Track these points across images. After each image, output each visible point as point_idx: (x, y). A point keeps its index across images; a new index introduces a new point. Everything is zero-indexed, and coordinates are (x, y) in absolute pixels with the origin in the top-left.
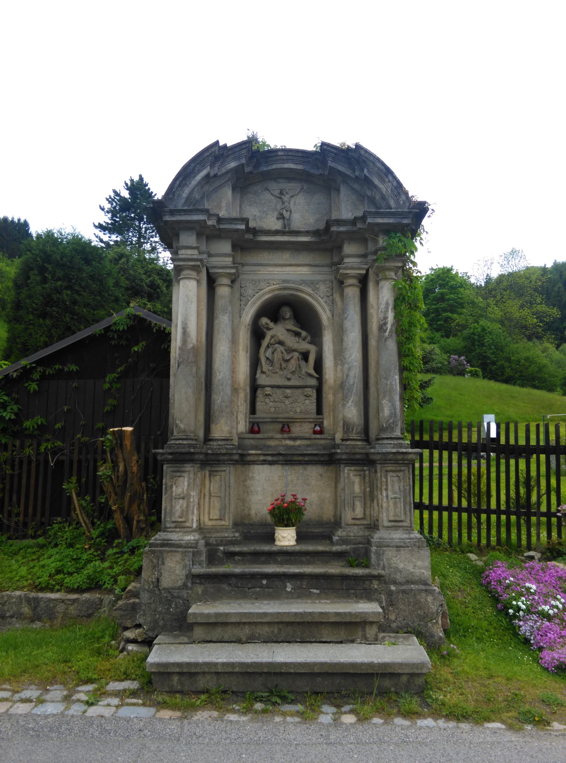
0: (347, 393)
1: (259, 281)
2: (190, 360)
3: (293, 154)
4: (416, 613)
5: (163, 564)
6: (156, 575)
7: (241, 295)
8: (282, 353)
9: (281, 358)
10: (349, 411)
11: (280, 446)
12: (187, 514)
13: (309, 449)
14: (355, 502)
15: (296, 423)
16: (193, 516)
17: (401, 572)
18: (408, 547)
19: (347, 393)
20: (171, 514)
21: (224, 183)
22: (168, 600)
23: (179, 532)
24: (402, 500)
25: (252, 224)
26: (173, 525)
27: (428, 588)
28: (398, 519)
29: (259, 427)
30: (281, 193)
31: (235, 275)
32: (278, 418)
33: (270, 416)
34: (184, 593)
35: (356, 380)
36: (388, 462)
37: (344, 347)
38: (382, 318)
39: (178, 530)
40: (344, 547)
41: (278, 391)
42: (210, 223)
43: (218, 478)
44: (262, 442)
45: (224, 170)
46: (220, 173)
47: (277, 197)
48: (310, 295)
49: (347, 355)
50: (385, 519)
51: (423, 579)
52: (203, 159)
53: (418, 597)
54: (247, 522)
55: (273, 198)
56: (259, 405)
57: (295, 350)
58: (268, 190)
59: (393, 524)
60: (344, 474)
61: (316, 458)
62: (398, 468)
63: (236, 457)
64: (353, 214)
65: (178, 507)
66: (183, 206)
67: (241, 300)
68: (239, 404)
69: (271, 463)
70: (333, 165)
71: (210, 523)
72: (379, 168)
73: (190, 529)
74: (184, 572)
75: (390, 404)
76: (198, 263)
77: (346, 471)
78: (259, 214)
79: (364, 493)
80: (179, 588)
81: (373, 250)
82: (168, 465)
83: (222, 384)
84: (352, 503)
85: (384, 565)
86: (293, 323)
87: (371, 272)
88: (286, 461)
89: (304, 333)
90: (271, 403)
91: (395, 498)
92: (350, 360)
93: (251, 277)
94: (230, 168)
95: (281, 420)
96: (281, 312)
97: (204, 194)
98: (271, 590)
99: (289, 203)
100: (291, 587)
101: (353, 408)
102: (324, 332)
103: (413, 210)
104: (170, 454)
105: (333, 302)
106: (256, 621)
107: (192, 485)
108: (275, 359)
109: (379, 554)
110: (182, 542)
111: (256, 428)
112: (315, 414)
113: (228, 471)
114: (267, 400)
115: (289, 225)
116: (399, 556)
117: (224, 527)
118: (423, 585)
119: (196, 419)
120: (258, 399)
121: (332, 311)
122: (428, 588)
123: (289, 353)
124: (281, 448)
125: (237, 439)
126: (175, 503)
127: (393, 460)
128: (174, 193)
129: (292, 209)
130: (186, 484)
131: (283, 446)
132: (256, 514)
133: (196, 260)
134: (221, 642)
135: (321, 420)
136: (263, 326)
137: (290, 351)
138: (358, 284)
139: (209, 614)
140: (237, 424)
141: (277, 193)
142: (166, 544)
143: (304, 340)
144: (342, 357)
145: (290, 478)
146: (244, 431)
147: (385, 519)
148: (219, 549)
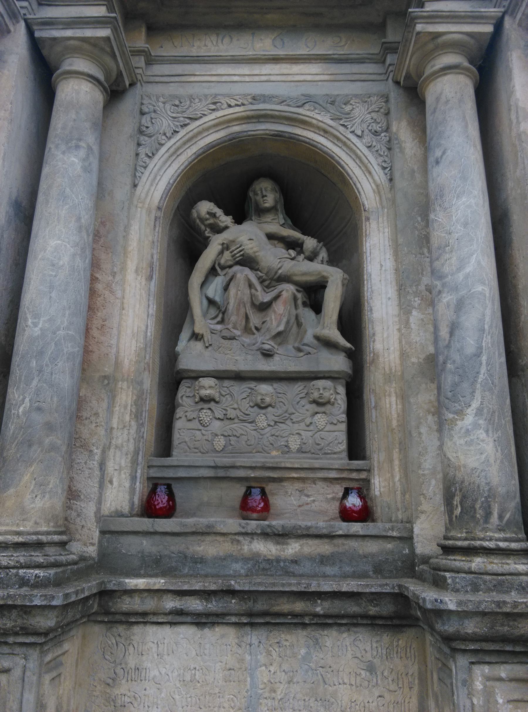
0: (456, 385)
1: (191, 98)
8: (251, 286)
9: (247, 298)
10: (469, 443)
11: (236, 560)
13: (329, 570)
15: (285, 484)
19: (456, 385)
29: (171, 496)
32: (233, 467)
33: (209, 460)
35: (487, 341)
60: (470, 695)
61: (353, 608)
67: (139, 145)
68: (115, 423)
77: (479, 685)
83: (41, 353)
86: (282, 221)
88: (250, 615)
89: (310, 243)
90: (217, 424)
92: (461, 276)
93: (172, 89)
95: (241, 473)
96: (251, 194)
102: (365, 226)
108: (232, 301)
111: (162, 500)
112: (345, 455)
113: (17, 672)
114: (205, 415)
120: (179, 412)
123: (268, 287)
124: (237, 566)
125: (97, 534)
131: (246, 560)
135: (363, 475)
136: (202, 220)
146: (126, 509)
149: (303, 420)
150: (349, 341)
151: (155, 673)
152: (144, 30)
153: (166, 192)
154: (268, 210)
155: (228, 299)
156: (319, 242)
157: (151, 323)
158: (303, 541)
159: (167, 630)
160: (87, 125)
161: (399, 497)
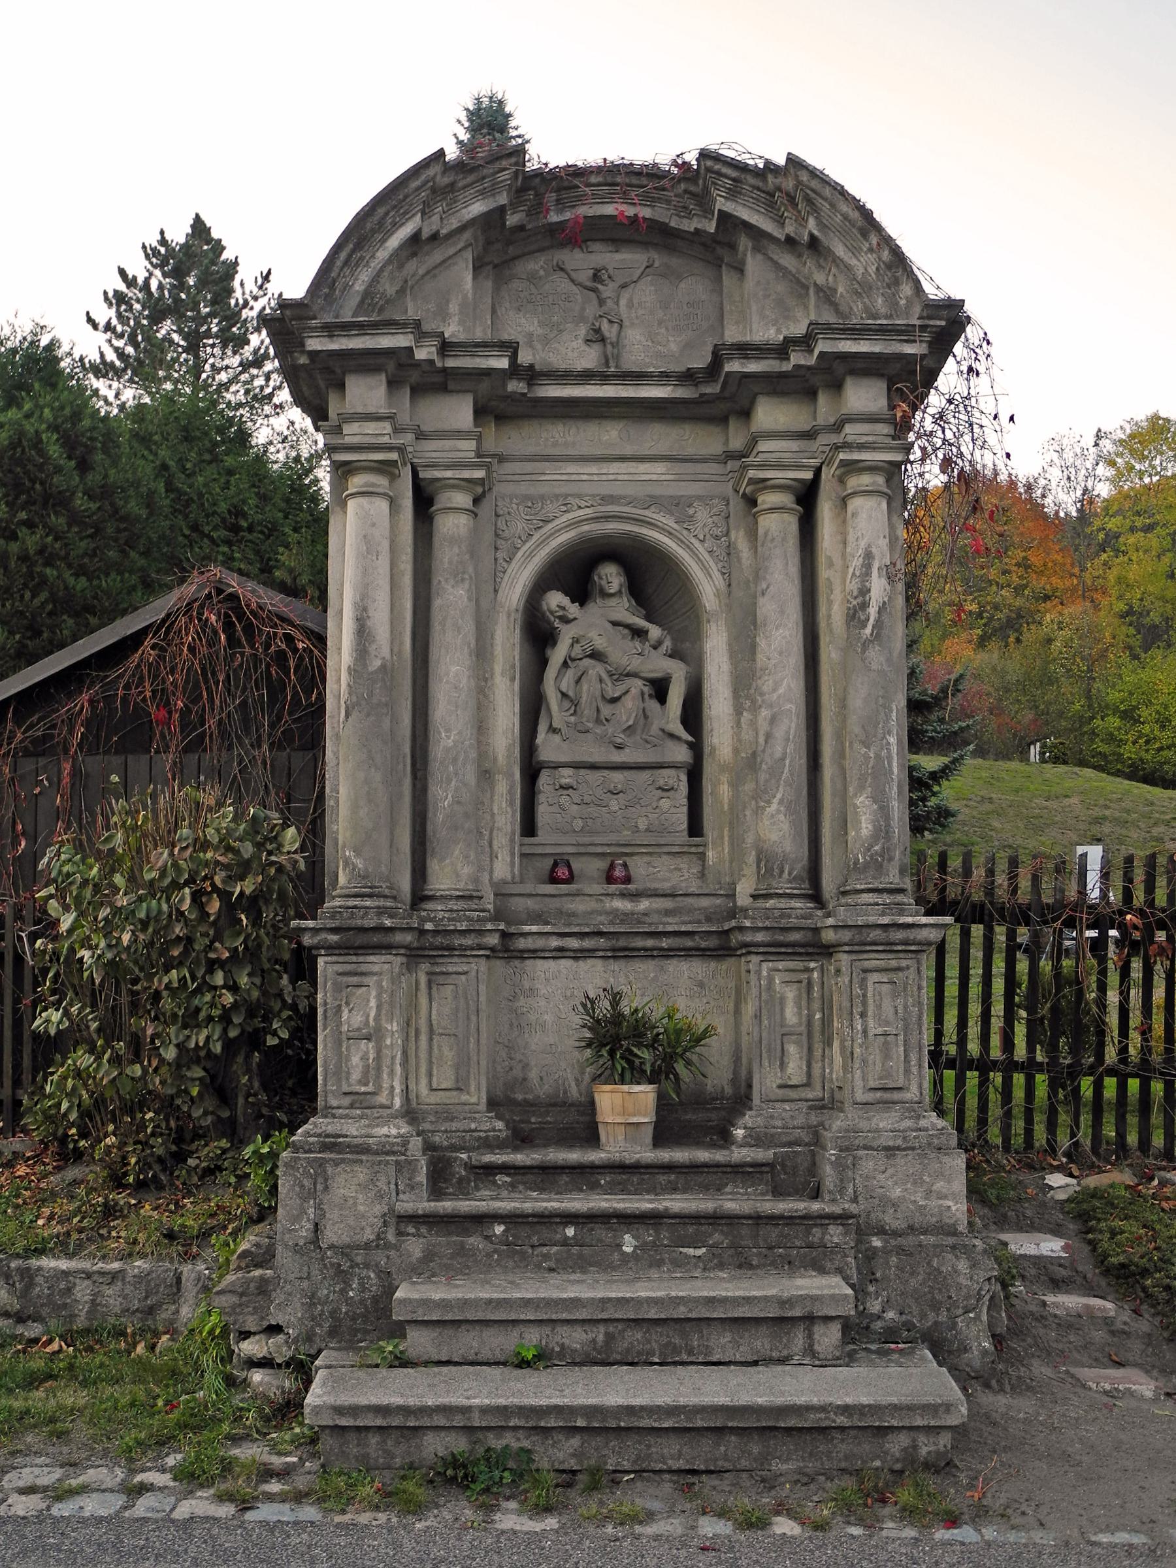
1: (542, 498)
2: (375, 701)
5: (326, 1188)
6: (312, 1216)
7: (497, 535)
9: (598, 693)
10: (774, 824)
11: (600, 913)
12: (378, 1077)
14: (786, 1046)
19: (767, 781)
21: (456, 254)
24: (901, 1038)
25: (524, 358)
26: (347, 1101)
30: (596, 277)
31: (483, 485)
35: (790, 748)
36: (868, 948)
37: (759, 664)
38: (855, 593)
40: (763, 1155)
42: (421, 354)
43: (448, 991)
45: (454, 223)
46: (444, 231)
47: (586, 288)
48: (670, 534)
49: (767, 684)
50: (859, 1083)
54: (519, 1097)
55: (575, 289)
56: (544, 813)
57: (635, 675)
58: (562, 269)
59: (879, 1094)
61: (689, 943)
62: (894, 963)
63: (493, 940)
64: (779, 331)
65: (355, 1060)
66: (354, 315)
67: (496, 549)
70: (729, 207)
71: (435, 1098)
72: (845, 217)
73: (389, 1111)
74: (378, 1209)
75: (875, 807)
76: (394, 456)
77: (765, 973)
78: (540, 331)
79: (809, 1024)
80: (367, 1246)
81: (832, 420)
82: (329, 959)
83: (455, 760)
84: (779, 1048)
87: (825, 473)
88: (614, 950)
89: (655, 632)
91: (886, 1035)
94: (471, 216)
96: (596, 578)
97: (406, 281)
99: (617, 303)
101: (781, 817)
102: (706, 626)
103: (931, 323)
104: (334, 930)
105: (730, 550)
107: (386, 1007)
110: (371, 1140)
112: (686, 833)
114: (564, 800)
115: (617, 357)
116: (890, 1171)
119: (391, 847)
120: (541, 798)
121: (727, 574)
126: (348, 1049)
127: (882, 944)
128: (334, 282)
129: (624, 316)
130: (373, 1003)
131: (607, 913)
132: (541, 1078)
133: (389, 448)
134: (472, 1364)
135: (701, 849)
136: (552, 613)
140: (491, 860)
141: (585, 276)
142: (331, 1144)
143: (655, 648)
144: (752, 691)
147: (859, 1083)
149: (650, 805)
150: (691, 735)
154: (612, 595)
155: (581, 693)
156: (663, 630)
158: (652, 899)
161: (727, 865)
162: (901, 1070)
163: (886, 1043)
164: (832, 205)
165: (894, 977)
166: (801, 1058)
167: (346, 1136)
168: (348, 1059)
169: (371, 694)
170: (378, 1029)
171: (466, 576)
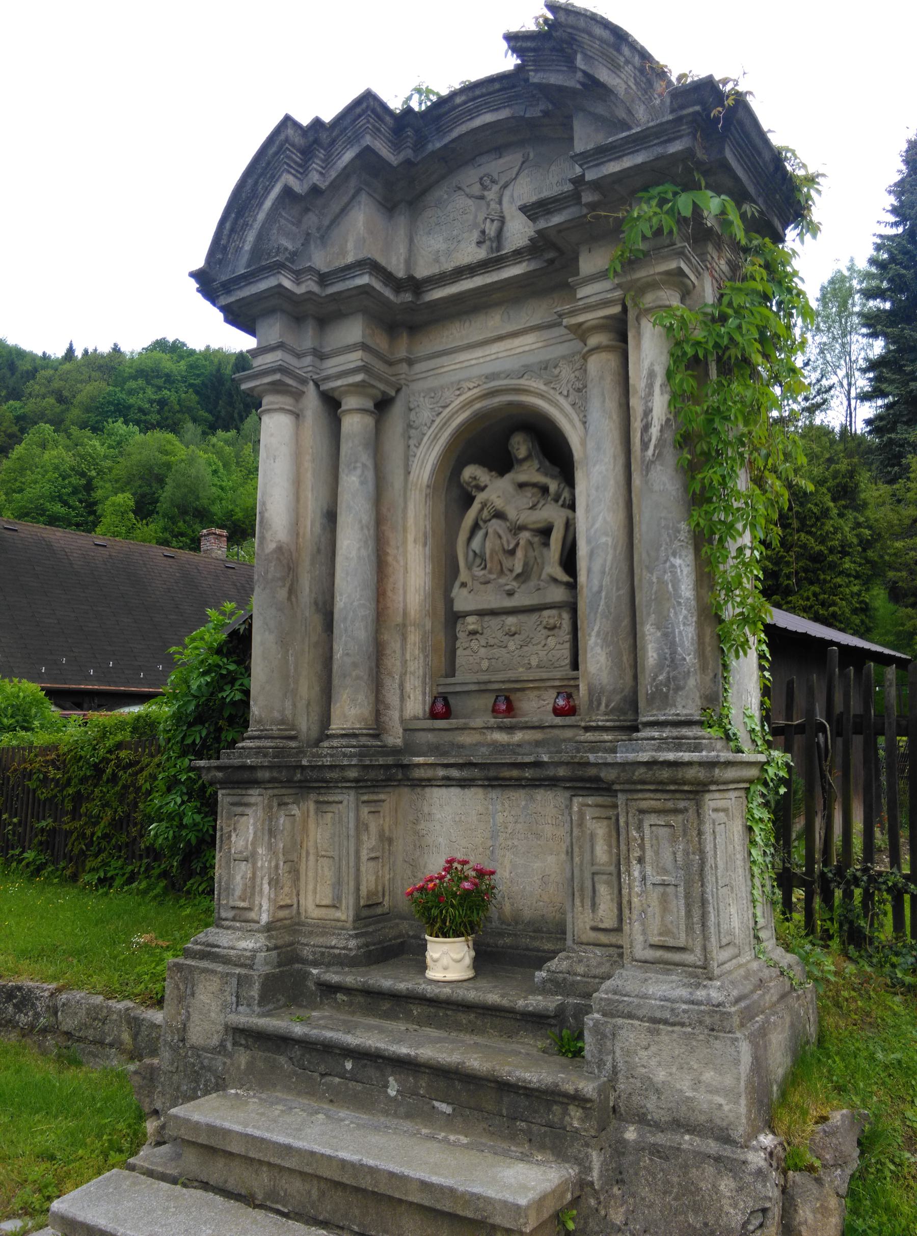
1: (442, 388)
2: (270, 576)
3: (484, 90)
4: (682, 1218)
5: (193, 994)
11: (483, 745)
12: (253, 894)
14: (598, 886)
16: (261, 897)
17: (657, 1091)
18: (683, 1025)
20: (229, 890)
22: (195, 1072)
23: (239, 929)
24: (681, 889)
26: (230, 914)
27: (727, 1151)
28: (671, 942)
32: (490, 682)
34: (219, 1063)
35: (607, 580)
39: (238, 924)
41: (493, 622)
44: (448, 737)
45: (333, 174)
50: (639, 938)
51: (718, 1122)
52: (268, 164)
53: (694, 1173)
55: (470, 202)
59: (659, 954)
62: (670, 805)
69: (463, 784)
71: (316, 913)
72: (601, 40)
77: (575, 809)
82: (224, 791)
83: (345, 619)
85: (614, 1067)
88: (488, 779)
90: (483, 650)
91: (664, 884)
95: (496, 686)
98: (359, 1087)
100: (396, 1087)
103: (685, 112)
106: (272, 1160)
109: (604, 1036)
110: (232, 952)
113: (345, 803)
114: (474, 645)
116: (653, 1048)
117: (340, 924)
118: (717, 1139)
122: (727, 1151)
124: (483, 750)
130: (251, 830)
131: (489, 745)
136: (468, 484)
137: (518, 529)
138: (613, 343)
139: (197, 1123)
145: (500, 818)
146: (421, 715)
147: (639, 938)
148: (310, 973)
151: (439, 816)
152: (405, 335)
153: (432, 473)
157: (428, 580)
159: (443, 791)
160: (360, 448)
162: (683, 927)
163: (664, 894)
164: (590, 34)
165: (672, 820)
166: (612, 900)
167: (219, 947)
168: (234, 878)
169: (267, 572)
170: (254, 854)
171: (359, 465)
